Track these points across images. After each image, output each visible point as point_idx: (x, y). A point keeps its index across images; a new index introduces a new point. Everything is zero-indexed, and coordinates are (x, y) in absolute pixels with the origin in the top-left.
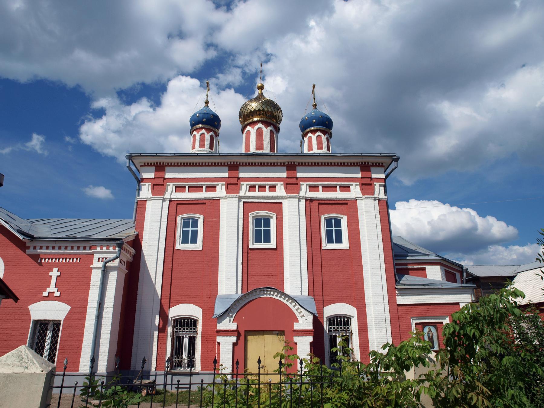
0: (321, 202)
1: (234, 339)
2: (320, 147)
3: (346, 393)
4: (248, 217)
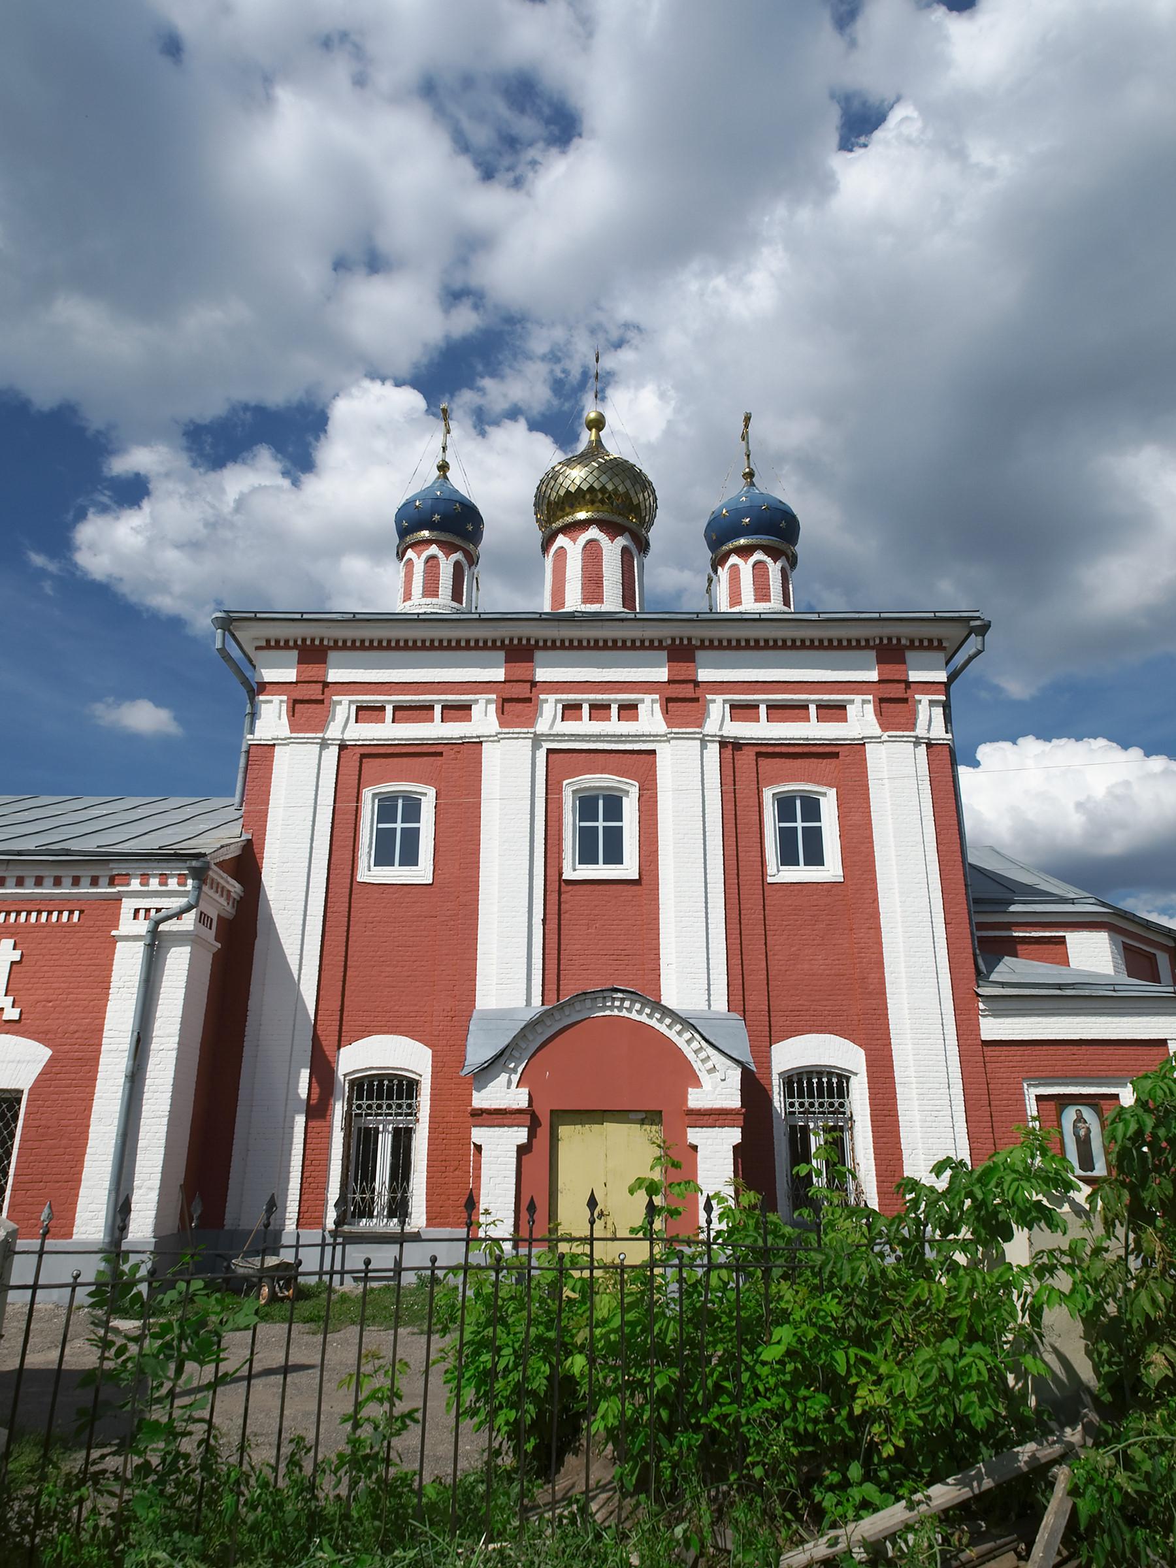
0: (763, 749)
1: (520, 1135)
2: (762, 593)
3: (834, 1296)
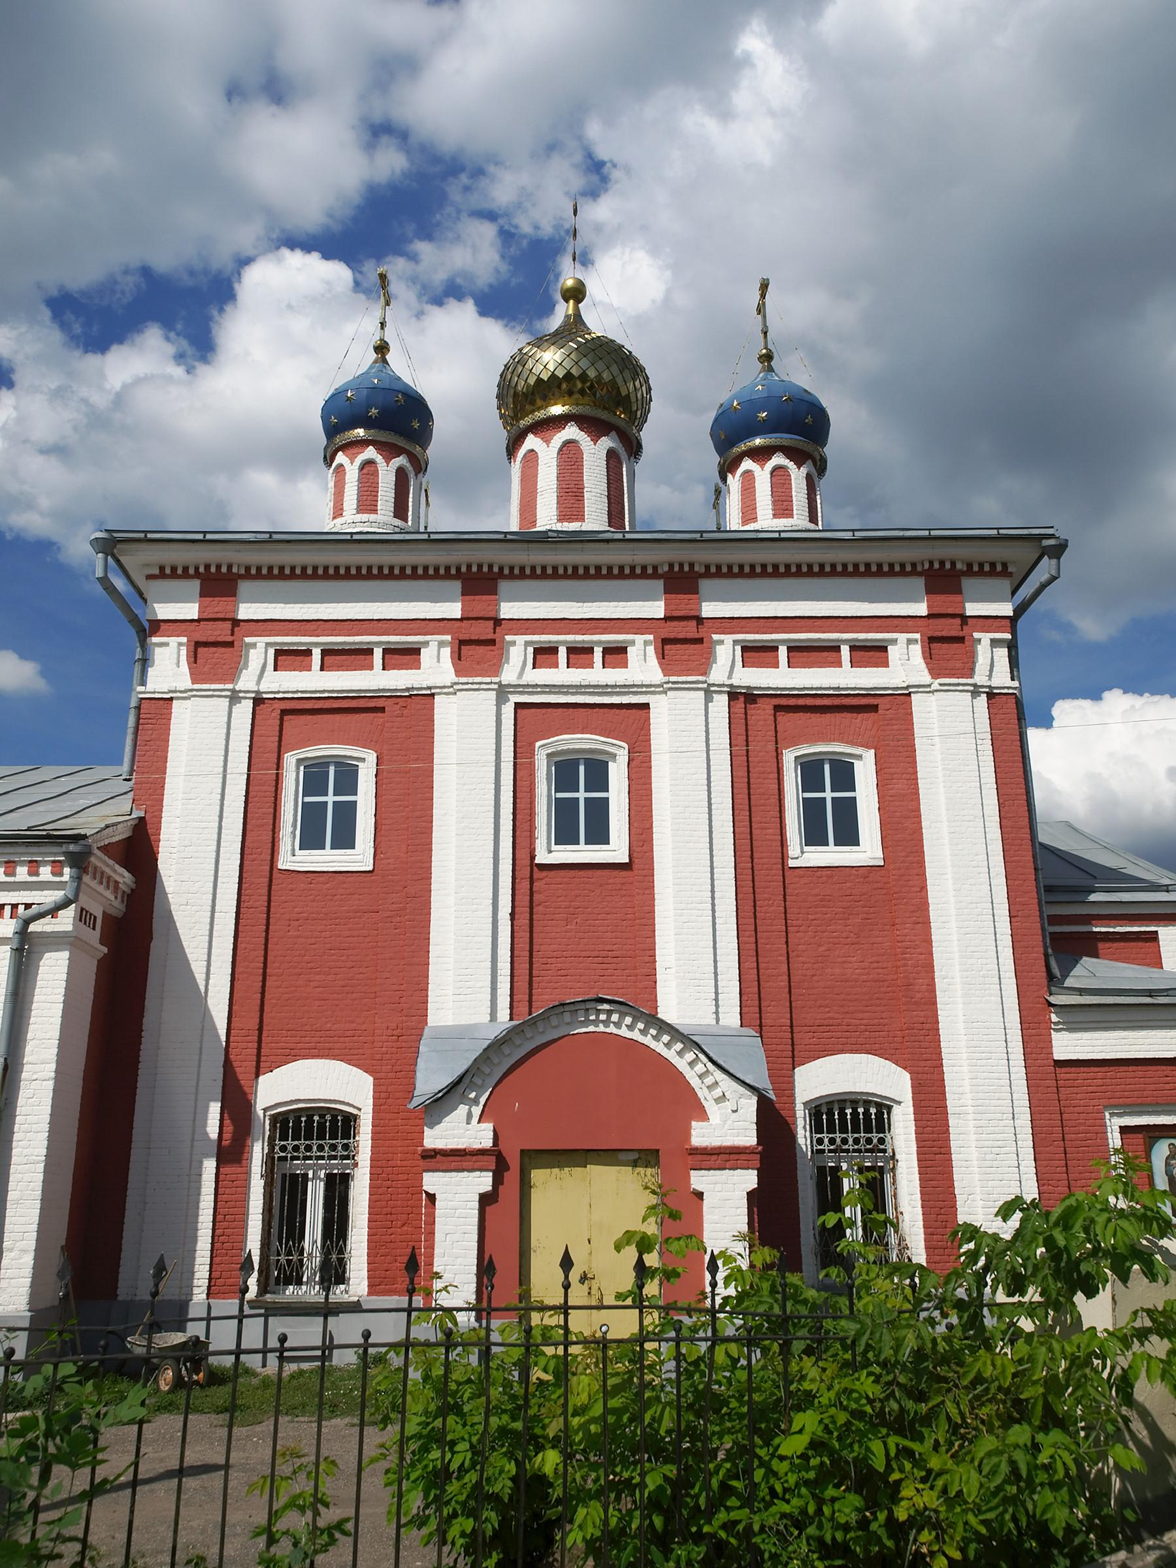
0: (783, 702)
1: (484, 1181)
2: (782, 507)
3: (869, 1374)
4: (532, 754)
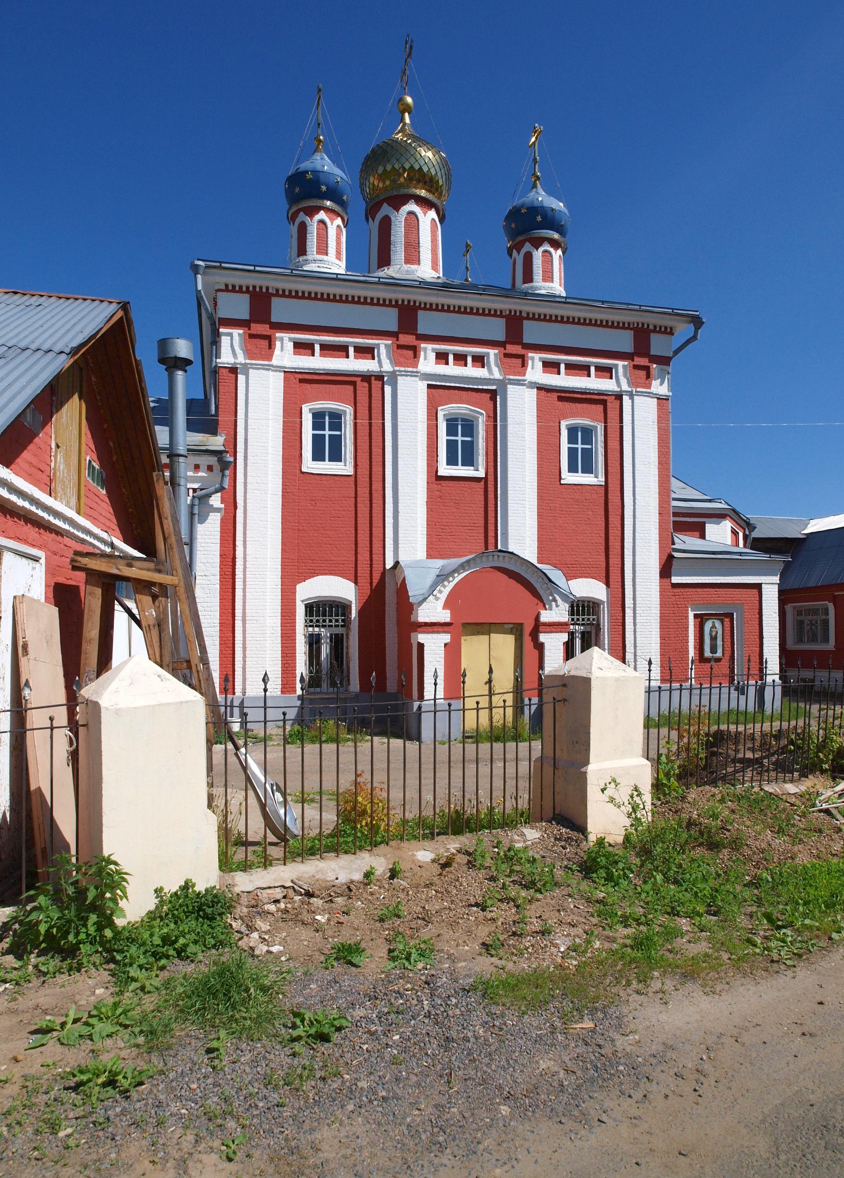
1: (446, 638)
